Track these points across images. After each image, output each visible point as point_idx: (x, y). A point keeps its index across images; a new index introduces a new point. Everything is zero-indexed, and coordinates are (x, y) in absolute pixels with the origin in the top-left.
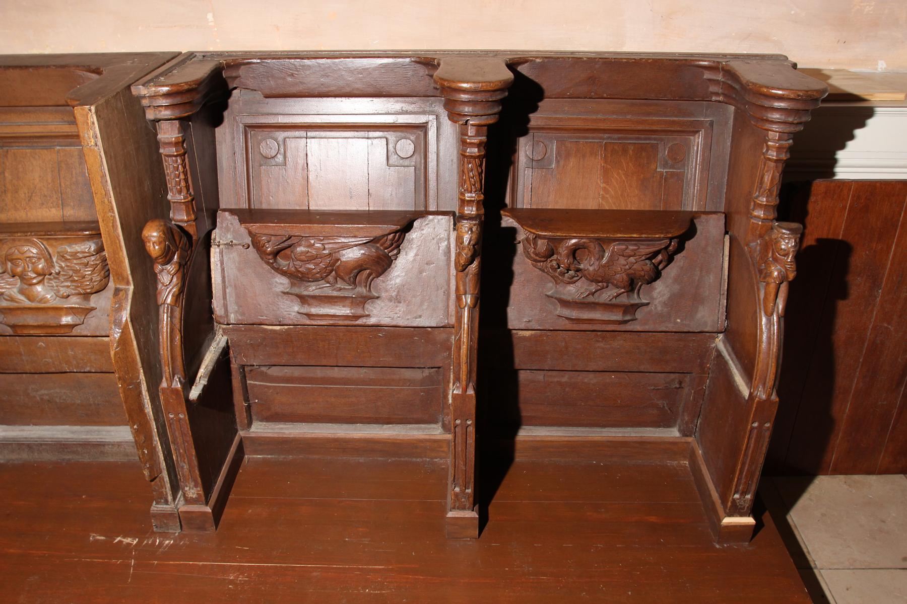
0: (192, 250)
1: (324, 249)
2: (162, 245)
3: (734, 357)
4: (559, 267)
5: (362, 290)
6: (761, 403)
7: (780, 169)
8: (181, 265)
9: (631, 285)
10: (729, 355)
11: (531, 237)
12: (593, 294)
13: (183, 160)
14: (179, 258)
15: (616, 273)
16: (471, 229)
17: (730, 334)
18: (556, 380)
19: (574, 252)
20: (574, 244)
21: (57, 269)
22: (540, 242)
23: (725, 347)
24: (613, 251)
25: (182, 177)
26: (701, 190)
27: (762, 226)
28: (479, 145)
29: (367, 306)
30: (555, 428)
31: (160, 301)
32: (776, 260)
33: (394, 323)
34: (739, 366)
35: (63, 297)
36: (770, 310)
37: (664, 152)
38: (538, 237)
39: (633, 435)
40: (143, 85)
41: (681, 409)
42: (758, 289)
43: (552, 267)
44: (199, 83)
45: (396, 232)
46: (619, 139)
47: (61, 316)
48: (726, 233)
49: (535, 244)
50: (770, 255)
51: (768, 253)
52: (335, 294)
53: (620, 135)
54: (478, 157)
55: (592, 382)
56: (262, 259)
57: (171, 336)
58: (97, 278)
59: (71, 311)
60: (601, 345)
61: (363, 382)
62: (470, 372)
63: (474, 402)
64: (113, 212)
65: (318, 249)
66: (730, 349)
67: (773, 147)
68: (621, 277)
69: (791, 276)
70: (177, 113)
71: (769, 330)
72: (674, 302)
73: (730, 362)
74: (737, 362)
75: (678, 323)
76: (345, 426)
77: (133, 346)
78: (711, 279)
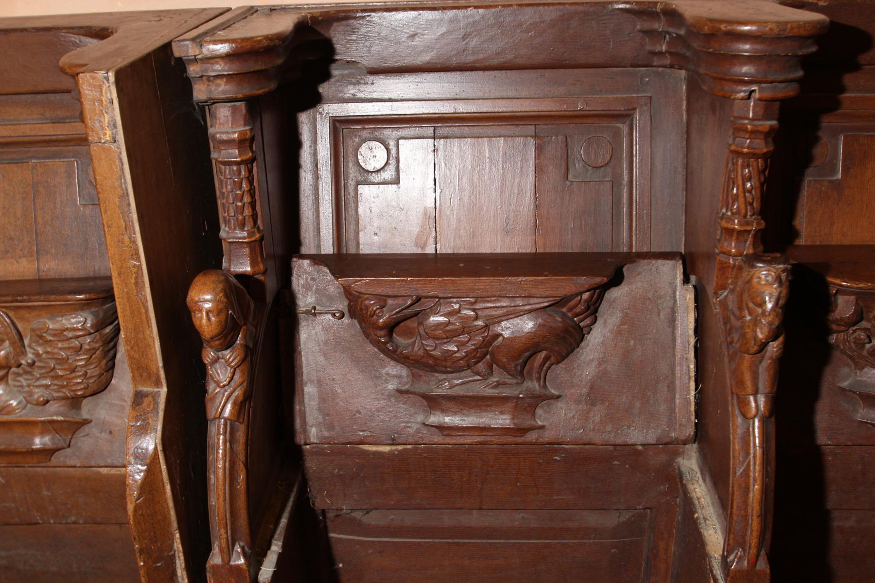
0: (268, 322)
1: (477, 318)
2: (223, 316)
5: (533, 385)
8: (249, 352)
13: (250, 171)
14: (245, 337)
21: (30, 356)
25: (247, 199)
29: (539, 411)
31: (211, 413)
33: (586, 439)
35: (38, 404)
40: (193, 40)
44: (280, 38)
47: (34, 435)
52: (489, 392)
56: (367, 335)
57: (231, 474)
58: (93, 371)
59: (49, 426)
61: (527, 533)
64: (138, 259)
65: (468, 317)
70: (247, 90)
77: (165, 493)
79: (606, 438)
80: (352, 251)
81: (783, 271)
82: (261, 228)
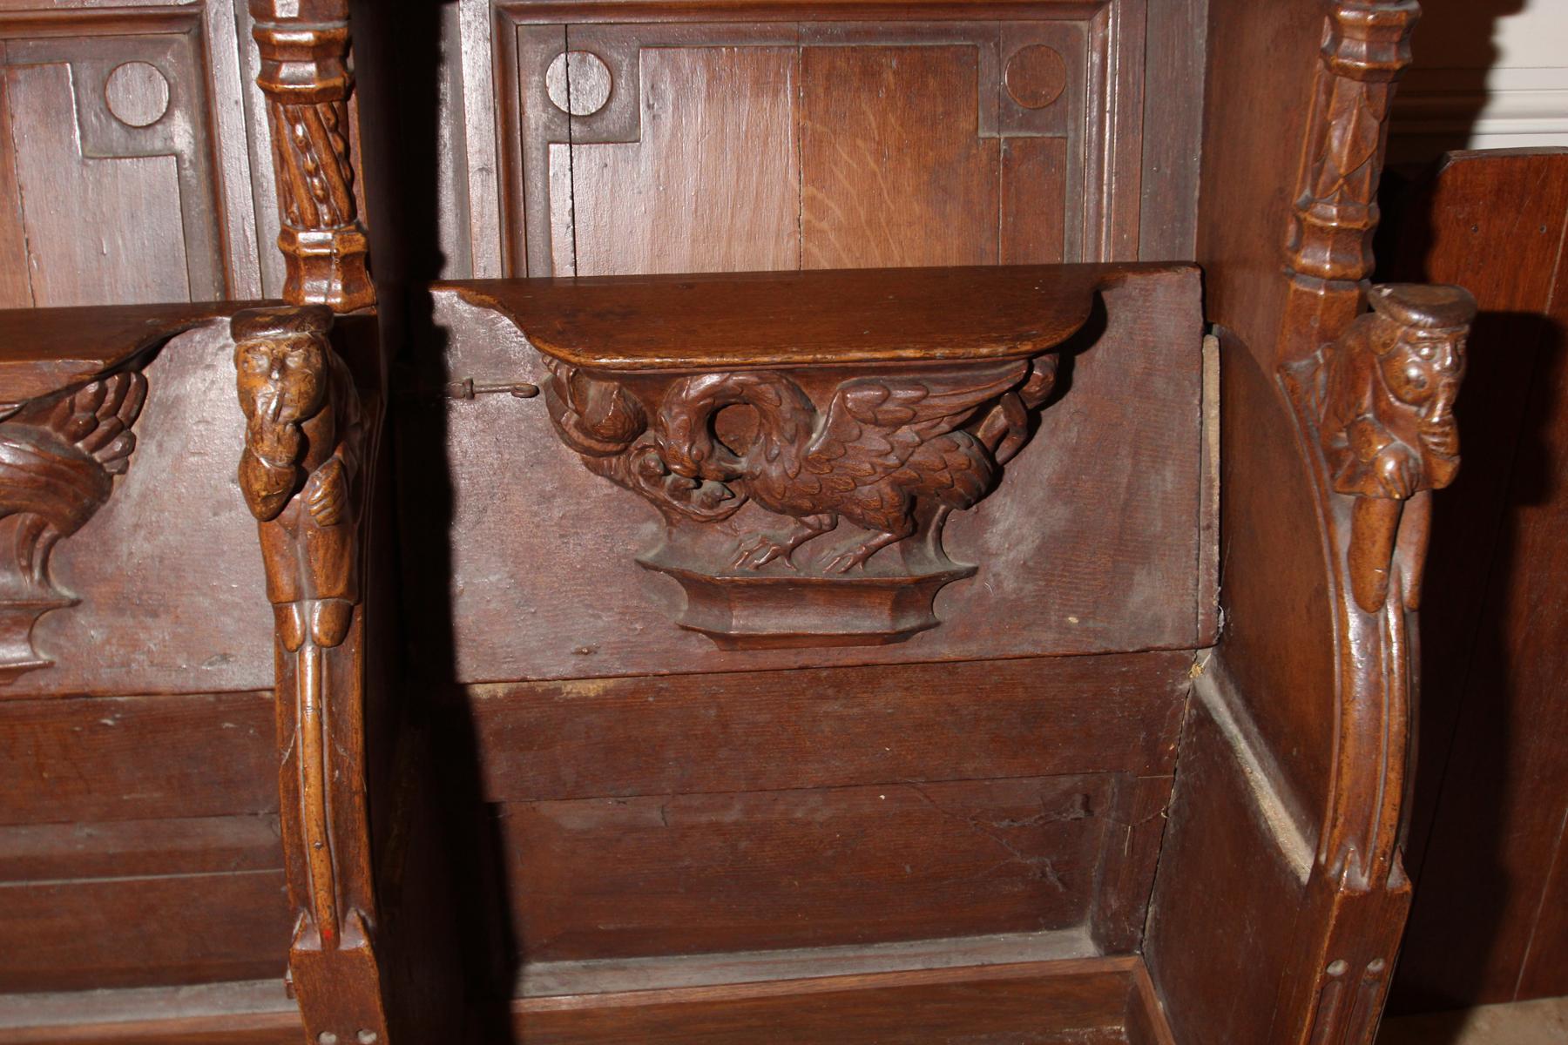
3: (1254, 730)
4: (667, 472)
6: (1357, 904)
7: (1381, 104)
9: (913, 514)
10: (1237, 720)
11: (563, 373)
12: (789, 553)
15: (857, 481)
16: (280, 364)
17: (1239, 655)
18: (704, 819)
19: (710, 417)
20: (711, 392)
22: (594, 390)
23: (1222, 691)
24: (843, 409)
26: (1121, 194)
27: (1329, 303)
28: (319, 51)
30: (721, 957)
32: (1387, 418)
34: (1272, 763)
36: (1373, 592)
37: (997, 77)
38: (584, 372)
39: (959, 961)
41: (1095, 874)
42: (1329, 520)
43: (644, 470)
45: (101, 376)
46: (849, 35)
48: (1207, 329)
49: (579, 397)
50: (1367, 400)
51: (1359, 398)
53: (852, 25)
54: (323, 95)
55: (819, 817)
60: (835, 707)
61: (109, 865)
62: (342, 877)
63: (373, 974)
66: (1238, 701)
67: (1354, 25)
68: (875, 492)
69: (1444, 473)
71: (1373, 657)
72: (1056, 560)
73: (1242, 746)
74: (1264, 749)
75: (1066, 628)
76: (57, 1000)
78: (1168, 479)
79: (179, 682)
80: (538, 272)
81: (295, 345)
82: (365, 226)
